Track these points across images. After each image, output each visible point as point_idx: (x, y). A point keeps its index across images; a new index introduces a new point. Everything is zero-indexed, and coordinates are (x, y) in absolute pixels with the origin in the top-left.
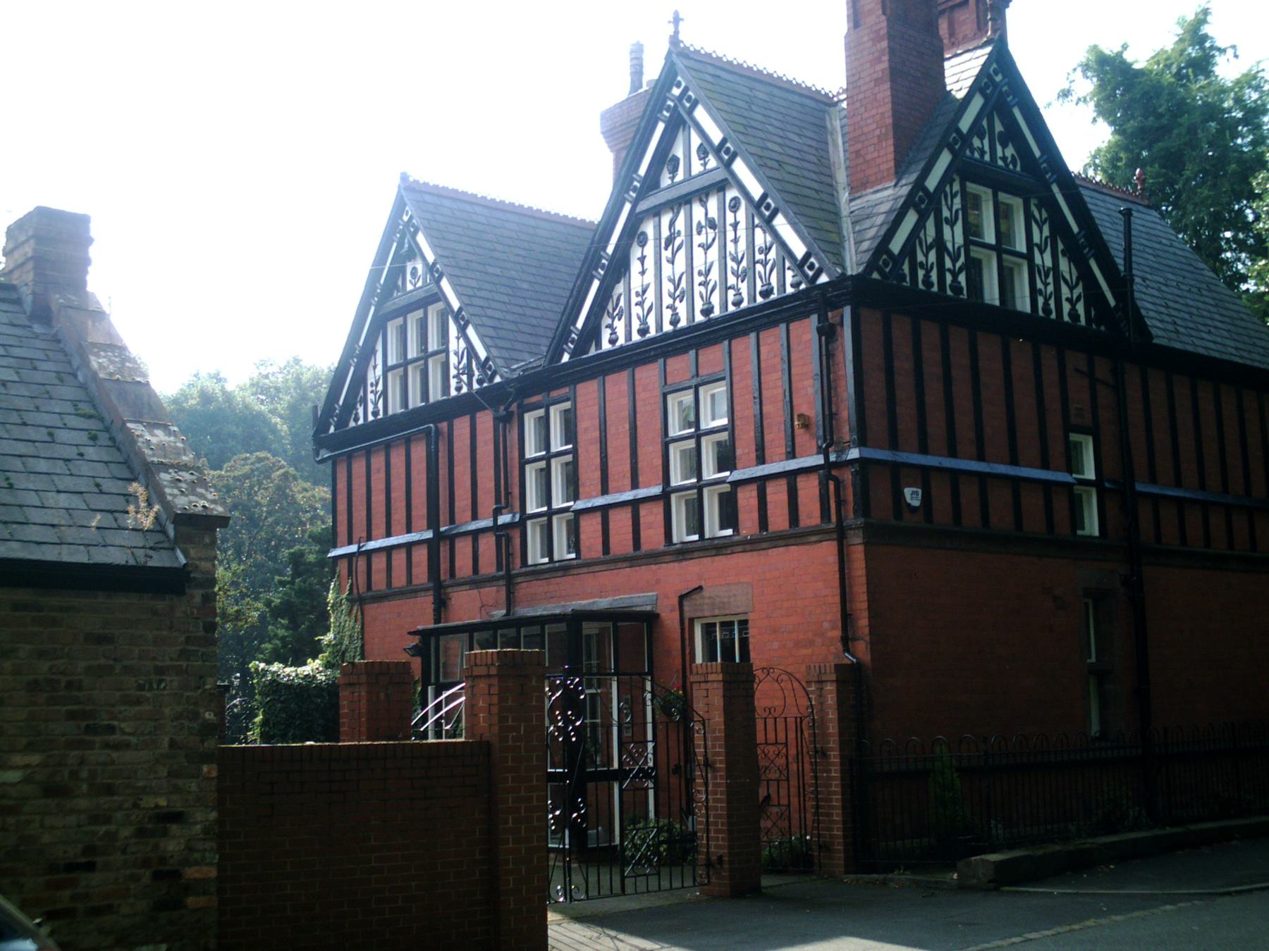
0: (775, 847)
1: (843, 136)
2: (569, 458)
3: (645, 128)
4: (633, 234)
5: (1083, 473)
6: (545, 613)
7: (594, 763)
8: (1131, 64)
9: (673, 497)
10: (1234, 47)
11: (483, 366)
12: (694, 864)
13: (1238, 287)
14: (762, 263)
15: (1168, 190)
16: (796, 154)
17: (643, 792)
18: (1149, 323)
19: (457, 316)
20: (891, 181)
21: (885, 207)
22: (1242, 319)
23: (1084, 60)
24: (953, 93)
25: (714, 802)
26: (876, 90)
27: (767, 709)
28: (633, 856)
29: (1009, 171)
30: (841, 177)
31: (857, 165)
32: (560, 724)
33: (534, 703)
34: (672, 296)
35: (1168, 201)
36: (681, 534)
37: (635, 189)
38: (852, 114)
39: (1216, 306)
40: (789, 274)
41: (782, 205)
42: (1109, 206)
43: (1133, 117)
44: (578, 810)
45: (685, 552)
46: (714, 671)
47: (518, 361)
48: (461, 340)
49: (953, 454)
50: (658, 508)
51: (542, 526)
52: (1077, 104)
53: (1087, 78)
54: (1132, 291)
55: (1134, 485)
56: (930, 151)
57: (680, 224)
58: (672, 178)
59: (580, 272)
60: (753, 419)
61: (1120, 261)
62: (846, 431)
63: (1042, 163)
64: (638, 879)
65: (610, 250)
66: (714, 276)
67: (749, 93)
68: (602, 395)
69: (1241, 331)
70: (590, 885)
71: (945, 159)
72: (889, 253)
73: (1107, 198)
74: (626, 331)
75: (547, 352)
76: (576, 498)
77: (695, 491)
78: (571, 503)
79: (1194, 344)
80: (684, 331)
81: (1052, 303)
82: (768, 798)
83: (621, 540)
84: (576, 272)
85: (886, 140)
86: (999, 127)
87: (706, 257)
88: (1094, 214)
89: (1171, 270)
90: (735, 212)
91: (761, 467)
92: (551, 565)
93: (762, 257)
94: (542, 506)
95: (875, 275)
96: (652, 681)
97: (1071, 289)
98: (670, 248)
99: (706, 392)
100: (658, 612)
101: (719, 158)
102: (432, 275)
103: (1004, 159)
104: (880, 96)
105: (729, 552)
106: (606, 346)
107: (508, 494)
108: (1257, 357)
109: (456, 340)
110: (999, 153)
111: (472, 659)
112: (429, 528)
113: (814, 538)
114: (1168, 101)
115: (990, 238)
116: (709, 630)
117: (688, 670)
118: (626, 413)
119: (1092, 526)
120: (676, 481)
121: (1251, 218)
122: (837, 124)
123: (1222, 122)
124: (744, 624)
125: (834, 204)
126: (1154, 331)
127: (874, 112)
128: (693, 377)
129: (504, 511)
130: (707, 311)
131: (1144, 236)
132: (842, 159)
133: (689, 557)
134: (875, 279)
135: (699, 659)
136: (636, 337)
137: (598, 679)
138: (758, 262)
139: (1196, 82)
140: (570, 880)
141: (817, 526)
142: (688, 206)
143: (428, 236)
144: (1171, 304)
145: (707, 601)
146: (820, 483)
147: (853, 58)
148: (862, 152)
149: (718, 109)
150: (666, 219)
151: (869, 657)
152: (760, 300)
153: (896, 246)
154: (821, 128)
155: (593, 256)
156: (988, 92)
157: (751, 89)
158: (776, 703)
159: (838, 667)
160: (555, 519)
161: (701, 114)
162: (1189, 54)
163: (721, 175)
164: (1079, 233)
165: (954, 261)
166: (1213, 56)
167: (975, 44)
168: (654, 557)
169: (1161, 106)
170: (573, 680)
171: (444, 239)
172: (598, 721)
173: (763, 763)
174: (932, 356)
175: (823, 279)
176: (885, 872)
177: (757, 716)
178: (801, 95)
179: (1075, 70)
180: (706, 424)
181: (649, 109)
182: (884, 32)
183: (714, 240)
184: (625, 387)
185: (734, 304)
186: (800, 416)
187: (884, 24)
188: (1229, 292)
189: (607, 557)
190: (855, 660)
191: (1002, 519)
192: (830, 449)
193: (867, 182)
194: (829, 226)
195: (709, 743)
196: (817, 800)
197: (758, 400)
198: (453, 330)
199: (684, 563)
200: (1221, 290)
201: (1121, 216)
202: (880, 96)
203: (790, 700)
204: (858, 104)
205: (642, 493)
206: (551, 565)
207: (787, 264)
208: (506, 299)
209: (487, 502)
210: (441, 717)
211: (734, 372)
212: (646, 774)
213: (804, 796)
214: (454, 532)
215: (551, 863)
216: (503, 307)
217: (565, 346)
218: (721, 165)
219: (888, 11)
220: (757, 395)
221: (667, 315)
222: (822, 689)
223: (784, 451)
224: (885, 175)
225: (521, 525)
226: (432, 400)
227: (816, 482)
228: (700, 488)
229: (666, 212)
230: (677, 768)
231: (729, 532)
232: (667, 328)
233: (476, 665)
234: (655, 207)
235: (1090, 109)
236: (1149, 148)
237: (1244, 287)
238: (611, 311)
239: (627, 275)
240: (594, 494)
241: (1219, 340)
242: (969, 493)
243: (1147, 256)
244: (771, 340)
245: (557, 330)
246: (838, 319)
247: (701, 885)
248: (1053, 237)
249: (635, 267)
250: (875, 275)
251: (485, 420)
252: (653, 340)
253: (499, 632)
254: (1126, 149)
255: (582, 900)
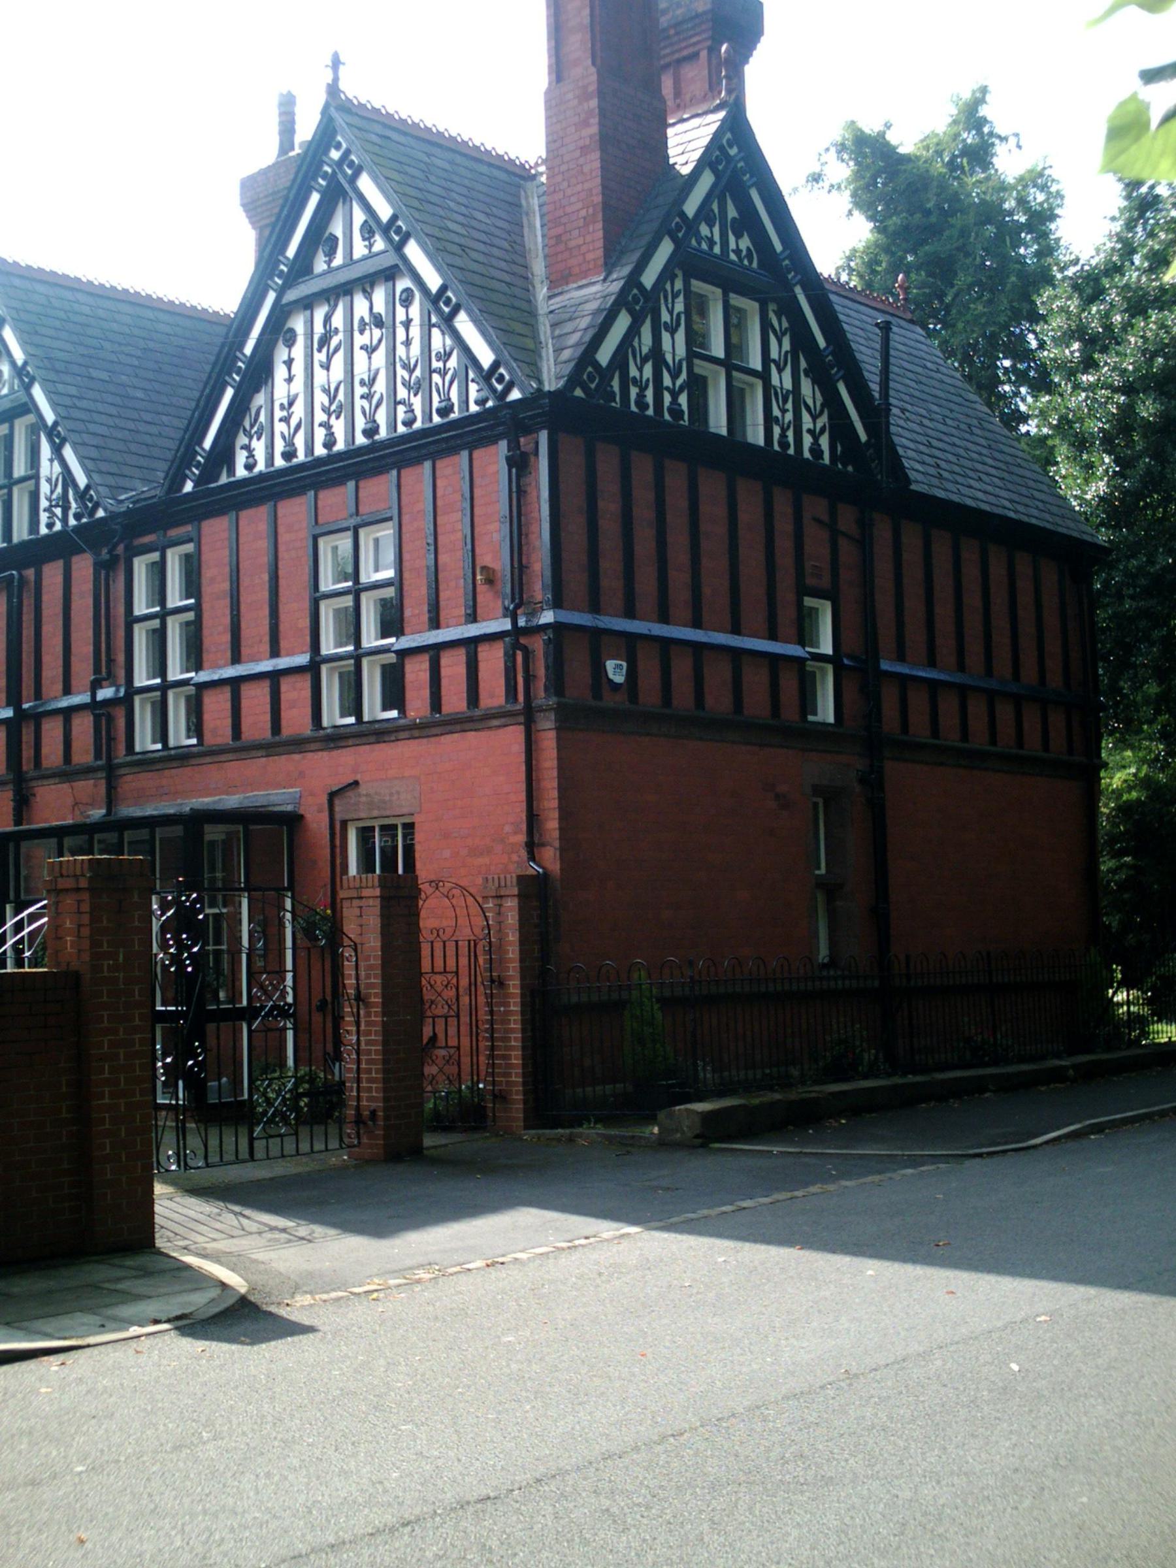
0: (441, 1098)
1: (542, 216)
2: (190, 616)
3: (296, 198)
4: (278, 330)
5: (818, 647)
6: (155, 813)
7: (217, 1001)
8: (895, 148)
9: (324, 669)
10: (1017, 135)
11: (82, 496)
12: (341, 1122)
13: (1016, 429)
14: (439, 373)
15: (936, 304)
16: (483, 237)
17: (277, 1034)
18: (906, 465)
19: (51, 432)
20: (599, 274)
21: (593, 306)
22: (1019, 466)
23: (839, 139)
24: (677, 167)
25: (366, 1044)
26: (582, 161)
27: (435, 932)
28: (265, 1113)
29: (742, 266)
30: (539, 267)
31: (556, 254)
32: (172, 950)
33: (137, 923)
34: (326, 410)
35: (935, 317)
36: (333, 716)
37: (281, 274)
38: (552, 189)
39: (990, 447)
40: (473, 388)
41: (465, 300)
42: (864, 317)
43: (896, 212)
44: (194, 1056)
45: (336, 739)
46: (364, 884)
47: (126, 490)
48: (56, 463)
49: (664, 618)
50: (305, 682)
51: (153, 704)
52: (830, 191)
53: (843, 161)
54: (888, 424)
55: (878, 662)
56: (647, 238)
57: (338, 320)
58: (329, 263)
59: (210, 377)
60: (425, 571)
61: (875, 387)
62: (539, 590)
63: (784, 260)
64: (271, 1141)
65: (248, 349)
66: (380, 387)
67: (426, 159)
68: (234, 536)
69: (1018, 480)
70: (210, 1150)
71: (666, 249)
72: (596, 365)
73: (862, 308)
74: (267, 453)
75: (165, 479)
76: (198, 667)
77: (352, 661)
78: (192, 674)
79: (959, 493)
80: (341, 456)
81: (790, 434)
82: (434, 1039)
83: (256, 723)
84: (204, 377)
85: (594, 222)
86: (732, 213)
87: (370, 363)
88: (845, 326)
89: (935, 401)
90: (407, 307)
91: (434, 632)
92: (165, 753)
93: (440, 364)
94: (154, 678)
95: (578, 392)
96: (293, 898)
97: (814, 418)
98: (325, 350)
99: (367, 535)
100: (301, 812)
101: (389, 240)
102: (22, 380)
103: (738, 252)
104: (586, 169)
105: (393, 738)
106: (241, 472)
107: (111, 661)
108: (1035, 512)
109: (48, 463)
110: (732, 245)
111: (57, 868)
112: (8, 705)
113: (495, 722)
114: (938, 195)
115: (718, 351)
116: (365, 835)
117: (338, 883)
118: (265, 560)
119: (826, 712)
120: (328, 647)
121: (1034, 344)
122: (535, 202)
123: (1002, 227)
124: (409, 827)
125: (529, 301)
126: (912, 475)
127: (579, 188)
128: (351, 516)
129: (104, 683)
130: (371, 432)
131: (905, 357)
132: (540, 246)
133: (343, 744)
134: (577, 397)
135: (353, 870)
136: (279, 462)
137: (224, 896)
138: (435, 371)
139: (971, 175)
140: (185, 1144)
141: (501, 707)
142: (348, 298)
143: (15, 329)
144: (935, 443)
145: (363, 799)
146: (506, 654)
147: (554, 120)
148: (564, 238)
149: (387, 178)
150: (319, 314)
151: (558, 867)
152: (437, 419)
153: (604, 356)
154: (515, 206)
155: (226, 358)
156: (720, 167)
157: (428, 155)
158: (445, 923)
159: (522, 880)
160: (171, 694)
161: (366, 184)
162: (964, 140)
163: (391, 259)
164: (826, 349)
165: (674, 377)
166: (993, 144)
167: (704, 107)
168: (298, 745)
169: (928, 200)
170: (189, 896)
171: (36, 333)
172: (224, 947)
173: (428, 995)
174: (643, 497)
175: (515, 395)
176: (572, 1126)
177: (421, 939)
178: (490, 165)
179: (827, 150)
180: (369, 575)
181: (300, 176)
182: (593, 88)
183: (380, 341)
184: (264, 527)
185: (405, 424)
186: (484, 568)
187: (594, 78)
188: (1006, 432)
189: (238, 744)
190: (541, 870)
191: (719, 701)
192: (519, 612)
193: (570, 275)
194: (518, 327)
195: (363, 973)
196: (492, 1039)
197: (432, 548)
198: (46, 449)
199: (335, 753)
200: (997, 429)
201: (878, 331)
202: (586, 169)
203: (463, 921)
204: (559, 178)
205: (283, 663)
206: (165, 753)
207: (471, 375)
208: (113, 411)
209: (83, 671)
210: (21, 941)
211: (404, 511)
212: (282, 1012)
213: (477, 1034)
214: (40, 710)
215: (160, 1123)
216: (111, 422)
217: (187, 472)
218: (390, 248)
219: (598, 62)
220: (431, 540)
221: (320, 434)
222: (500, 905)
223: (463, 612)
224: (591, 266)
225: (126, 702)
226: (15, 540)
227: (501, 653)
228: (357, 658)
229: (320, 305)
230: (323, 1004)
231: (394, 714)
232: (319, 451)
233: (62, 876)
234: (307, 297)
235: (844, 199)
236: (914, 251)
237: (1023, 429)
238: (248, 427)
239: (270, 384)
240: (222, 662)
241: (989, 489)
242: (682, 667)
243: (908, 382)
244: (449, 471)
245: (177, 451)
246: (532, 445)
247: (349, 1147)
248: (794, 352)
249: (280, 372)
250: (578, 392)
251: (83, 566)
252: (302, 467)
253: (97, 837)
254: (887, 250)
255: (199, 1168)
